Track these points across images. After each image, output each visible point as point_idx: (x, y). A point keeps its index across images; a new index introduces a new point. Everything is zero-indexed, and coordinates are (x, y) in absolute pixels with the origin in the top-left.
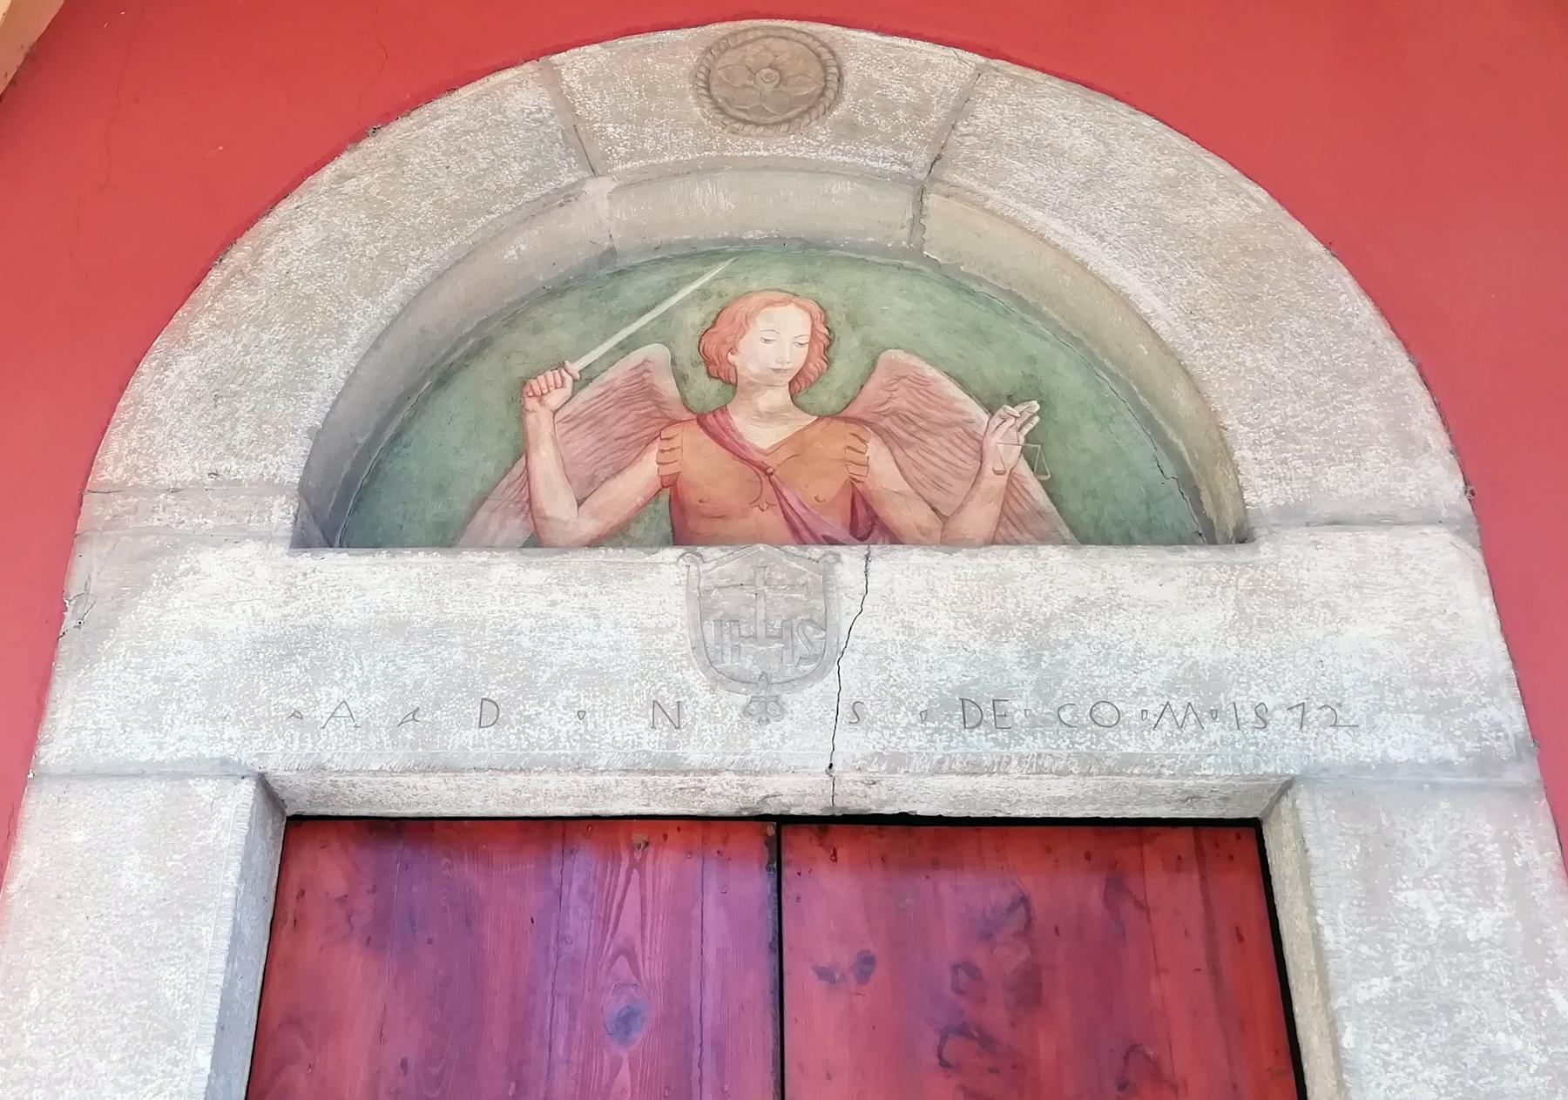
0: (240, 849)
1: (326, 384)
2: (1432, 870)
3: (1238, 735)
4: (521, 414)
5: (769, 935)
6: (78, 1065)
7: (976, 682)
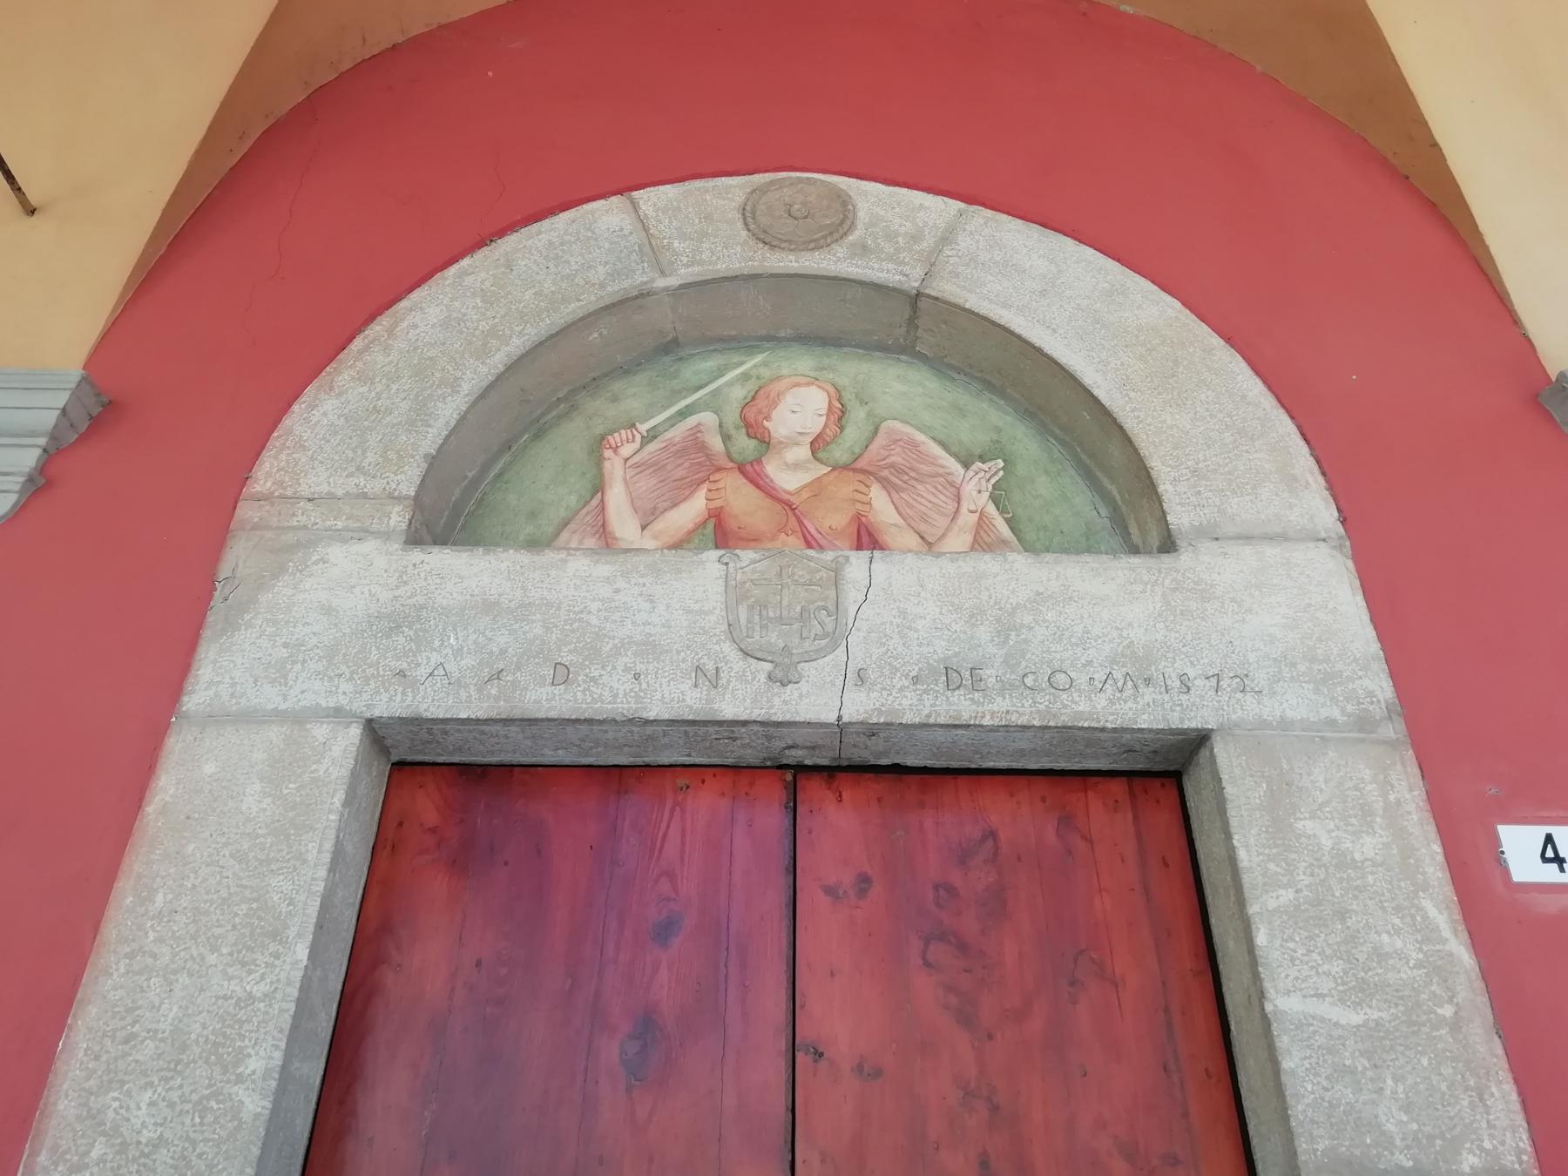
0: (346, 780)
1: (441, 422)
2: (1327, 803)
3: (1166, 697)
4: (599, 462)
5: (787, 861)
6: (192, 957)
7: (957, 655)
